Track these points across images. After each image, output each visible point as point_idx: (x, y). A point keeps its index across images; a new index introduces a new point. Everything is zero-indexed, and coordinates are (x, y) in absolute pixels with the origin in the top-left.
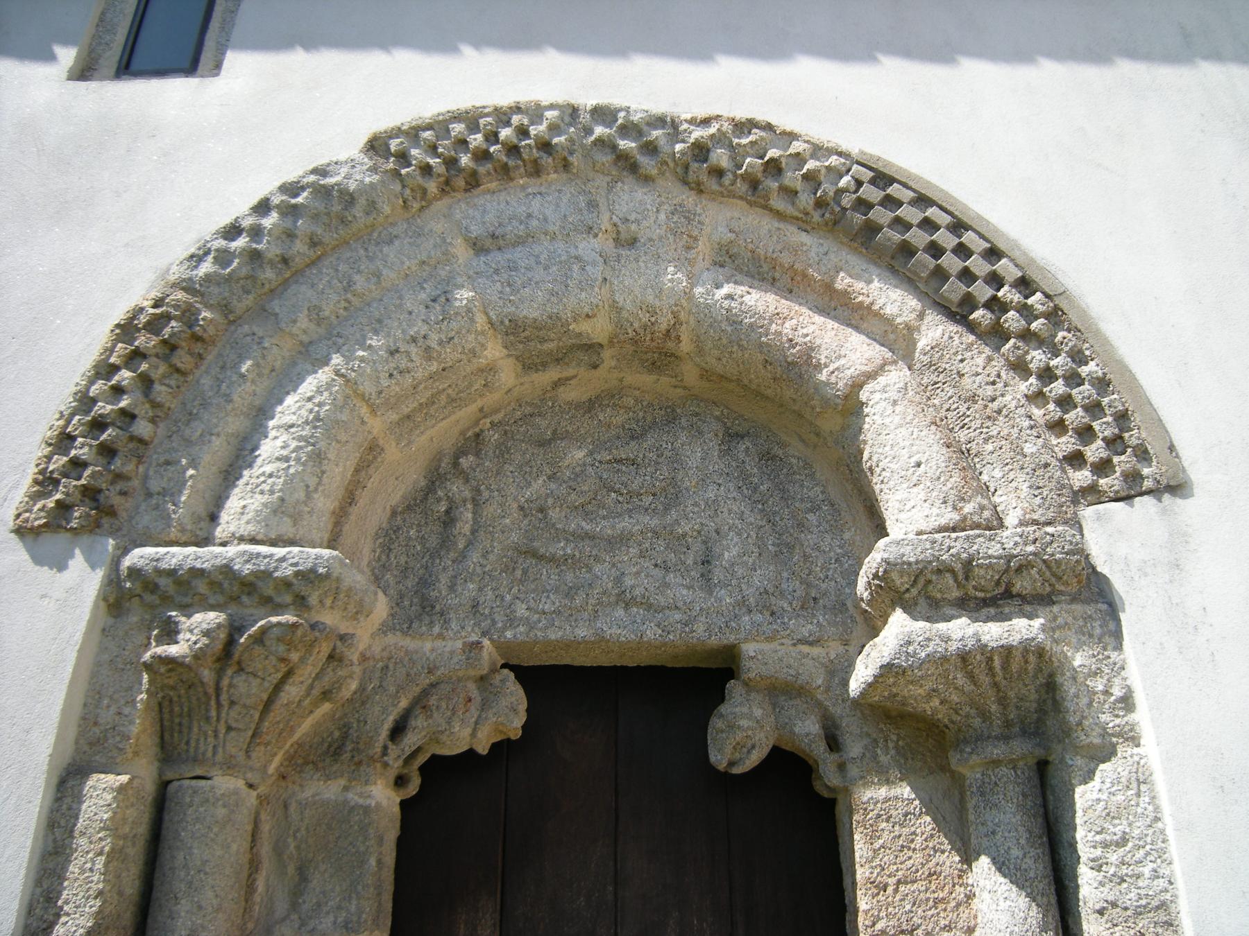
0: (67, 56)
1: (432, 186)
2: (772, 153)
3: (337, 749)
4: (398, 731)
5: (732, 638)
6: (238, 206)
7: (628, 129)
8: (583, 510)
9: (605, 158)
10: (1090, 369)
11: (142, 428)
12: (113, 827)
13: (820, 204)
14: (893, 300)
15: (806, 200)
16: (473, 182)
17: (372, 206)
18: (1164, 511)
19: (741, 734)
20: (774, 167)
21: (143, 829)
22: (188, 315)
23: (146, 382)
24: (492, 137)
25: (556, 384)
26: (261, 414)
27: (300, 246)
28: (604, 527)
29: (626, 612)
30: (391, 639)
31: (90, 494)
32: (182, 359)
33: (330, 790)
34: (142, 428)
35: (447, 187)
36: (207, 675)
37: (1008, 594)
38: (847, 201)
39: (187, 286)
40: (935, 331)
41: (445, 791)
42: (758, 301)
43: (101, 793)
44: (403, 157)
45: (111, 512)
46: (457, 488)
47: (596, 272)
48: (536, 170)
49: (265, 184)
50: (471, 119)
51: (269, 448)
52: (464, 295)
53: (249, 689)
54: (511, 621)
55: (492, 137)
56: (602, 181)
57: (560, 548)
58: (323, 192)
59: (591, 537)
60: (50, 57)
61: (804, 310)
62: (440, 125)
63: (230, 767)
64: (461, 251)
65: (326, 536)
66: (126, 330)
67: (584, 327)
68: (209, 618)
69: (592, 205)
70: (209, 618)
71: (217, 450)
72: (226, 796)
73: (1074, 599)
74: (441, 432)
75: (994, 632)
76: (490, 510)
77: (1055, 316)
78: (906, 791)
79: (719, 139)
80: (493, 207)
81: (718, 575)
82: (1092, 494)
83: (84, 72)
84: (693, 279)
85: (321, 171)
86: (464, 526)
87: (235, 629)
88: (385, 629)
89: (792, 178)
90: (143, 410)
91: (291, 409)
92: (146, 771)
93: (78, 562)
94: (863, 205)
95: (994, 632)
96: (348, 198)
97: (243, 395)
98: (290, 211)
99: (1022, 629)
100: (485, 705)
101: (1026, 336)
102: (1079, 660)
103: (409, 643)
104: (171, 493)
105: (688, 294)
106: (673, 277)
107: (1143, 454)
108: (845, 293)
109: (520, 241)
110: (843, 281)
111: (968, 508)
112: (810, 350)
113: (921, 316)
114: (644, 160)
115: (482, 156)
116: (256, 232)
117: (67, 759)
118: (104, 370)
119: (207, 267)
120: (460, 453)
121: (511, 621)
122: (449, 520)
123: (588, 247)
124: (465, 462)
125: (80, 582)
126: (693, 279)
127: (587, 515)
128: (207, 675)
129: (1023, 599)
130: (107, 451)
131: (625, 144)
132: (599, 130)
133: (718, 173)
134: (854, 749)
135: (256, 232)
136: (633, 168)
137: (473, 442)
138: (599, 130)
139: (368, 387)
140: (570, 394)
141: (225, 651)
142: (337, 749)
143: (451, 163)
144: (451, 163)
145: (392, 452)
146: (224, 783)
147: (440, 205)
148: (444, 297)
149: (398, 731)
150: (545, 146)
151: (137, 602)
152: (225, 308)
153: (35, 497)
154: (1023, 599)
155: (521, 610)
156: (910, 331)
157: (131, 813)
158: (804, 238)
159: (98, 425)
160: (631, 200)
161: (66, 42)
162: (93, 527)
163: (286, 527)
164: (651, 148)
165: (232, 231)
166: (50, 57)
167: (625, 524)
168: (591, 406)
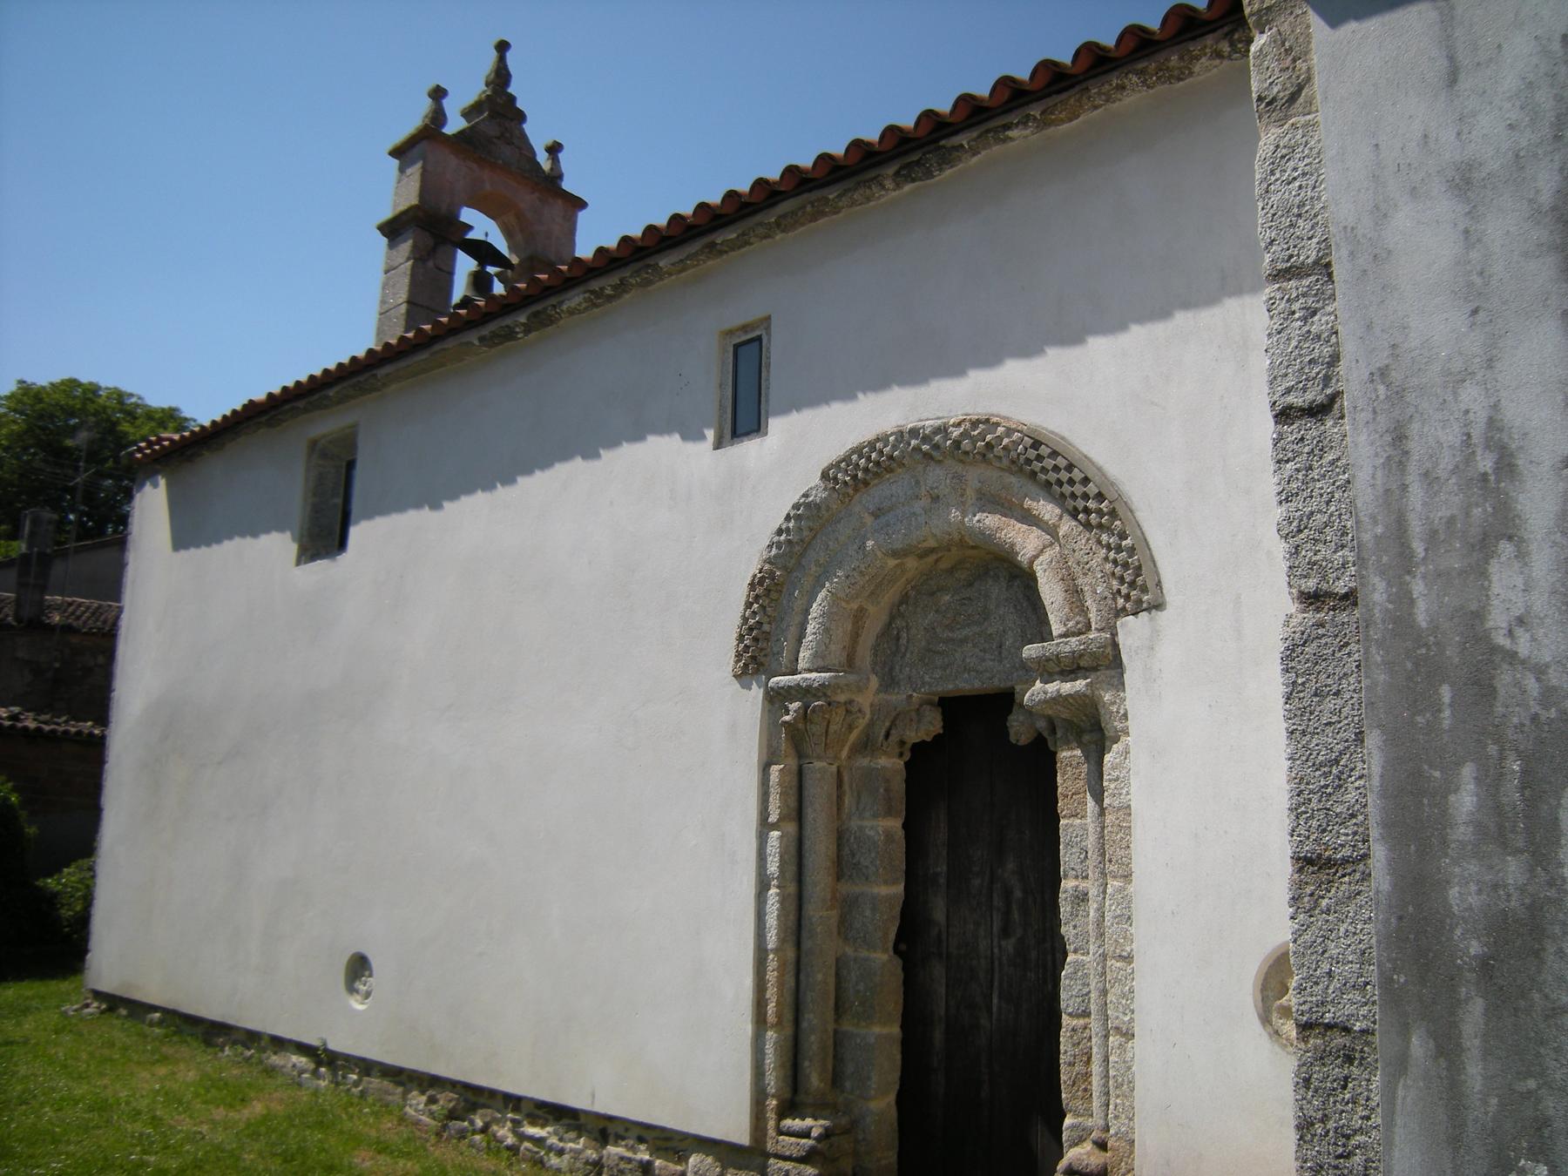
0: (710, 434)
1: (851, 492)
2: (989, 437)
3: (866, 745)
4: (887, 736)
5: (1009, 684)
6: (779, 521)
7: (926, 439)
8: (950, 628)
9: (918, 457)
10: (1127, 542)
11: (766, 627)
12: (780, 784)
13: (1013, 462)
14: (1047, 510)
15: (1005, 462)
16: (866, 484)
17: (828, 508)
18: (1151, 619)
19: (1019, 730)
20: (989, 446)
21: (795, 783)
22: (771, 574)
23: (763, 607)
24: (869, 459)
25: (937, 561)
26: (807, 612)
27: (806, 533)
28: (957, 635)
29: (970, 676)
30: (881, 695)
31: (753, 658)
32: (774, 595)
33: (864, 762)
34: (766, 627)
35: (856, 490)
36: (801, 726)
37: (1079, 668)
38: (1022, 458)
39: (768, 561)
40: (1067, 526)
41: (920, 758)
42: (990, 520)
43: (775, 769)
44: (835, 479)
45: (762, 664)
46: (899, 623)
47: (921, 519)
48: (890, 470)
49: (786, 508)
50: (858, 450)
51: (810, 629)
52: (870, 543)
53: (817, 729)
54: (923, 684)
55: (869, 459)
56: (920, 468)
57: (941, 647)
58: (808, 506)
59: (953, 640)
60: (703, 437)
61: (1013, 521)
62: (846, 459)
63: (819, 758)
64: (869, 520)
65: (843, 659)
66: (752, 586)
67: (925, 545)
68: (797, 705)
69: (917, 482)
70: (797, 705)
71: (793, 630)
72: (821, 768)
73: (1108, 668)
74: (890, 596)
75: (1067, 687)
76: (913, 631)
77: (1113, 514)
78: (1078, 752)
79: (965, 434)
80: (879, 493)
81: (1005, 653)
82: (1121, 612)
83: (718, 445)
84: (964, 514)
85: (806, 495)
86: (903, 641)
87: (806, 707)
88: (878, 691)
89: (998, 450)
90: (766, 619)
91: (815, 610)
92: (793, 763)
93: (754, 686)
94: (1028, 461)
95: (1067, 687)
96: (817, 506)
97: (798, 605)
98: (798, 518)
99: (1080, 685)
100: (919, 721)
101: (1100, 526)
102: (1107, 697)
103: (888, 697)
104: (780, 653)
105: (962, 522)
106: (955, 514)
107: (1144, 590)
108: (1029, 510)
109: (891, 509)
110: (1028, 503)
111: (1070, 624)
112: (1013, 545)
113: (1061, 518)
114: (934, 453)
115: (866, 470)
116: (788, 529)
117: (765, 758)
118: (749, 605)
119: (774, 551)
120: (901, 603)
121: (923, 684)
122: (898, 638)
123: (917, 507)
124: (902, 608)
125: (756, 693)
126: (964, 514)
127: (952, 630)
128: (801, 726)
129: (1086, 669)
130: (756, 639)
131: (925, 447)
132: (913, 442)
133: (966, 453)
134: (1059, 735)
135: (788, 529)
136: (932, 458)
137: (904, 599)
138: (913, 442)
139: (841, 595)
140: (943, 565)
141: (804, 714)
142: (866, 745)
143: (854, 477)
144: (854, 477)
145: (871, 609)
146: (818, 764)
147: (857, 497)
148: (862, 547)
149: (887, 736)
150: (891, 457)
151: (776, 699)
152: (784, 568)
153: (737, 662)
154: (1086, 669)
155: (927, 678)
156: (1056, 527)
157: (787, 779)
158: (1013, 479)
159: (751, 629)
160: (936, 476)
161: (709, 427)
162: (757, 672)
163: (820, 663)
164: (936, 447)
165: (780, 532)
166: (703, 437)
167: (966, 632)
168: (951, 571)
